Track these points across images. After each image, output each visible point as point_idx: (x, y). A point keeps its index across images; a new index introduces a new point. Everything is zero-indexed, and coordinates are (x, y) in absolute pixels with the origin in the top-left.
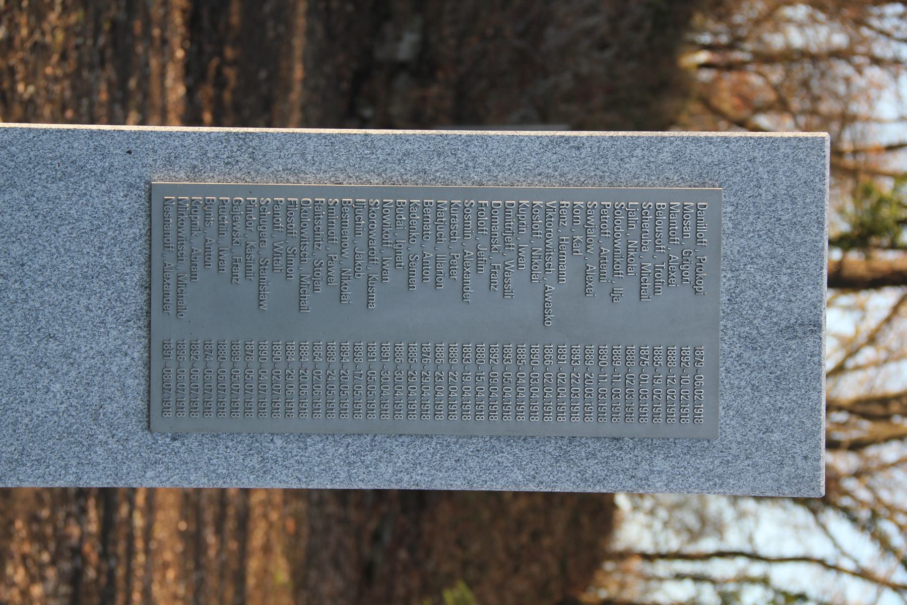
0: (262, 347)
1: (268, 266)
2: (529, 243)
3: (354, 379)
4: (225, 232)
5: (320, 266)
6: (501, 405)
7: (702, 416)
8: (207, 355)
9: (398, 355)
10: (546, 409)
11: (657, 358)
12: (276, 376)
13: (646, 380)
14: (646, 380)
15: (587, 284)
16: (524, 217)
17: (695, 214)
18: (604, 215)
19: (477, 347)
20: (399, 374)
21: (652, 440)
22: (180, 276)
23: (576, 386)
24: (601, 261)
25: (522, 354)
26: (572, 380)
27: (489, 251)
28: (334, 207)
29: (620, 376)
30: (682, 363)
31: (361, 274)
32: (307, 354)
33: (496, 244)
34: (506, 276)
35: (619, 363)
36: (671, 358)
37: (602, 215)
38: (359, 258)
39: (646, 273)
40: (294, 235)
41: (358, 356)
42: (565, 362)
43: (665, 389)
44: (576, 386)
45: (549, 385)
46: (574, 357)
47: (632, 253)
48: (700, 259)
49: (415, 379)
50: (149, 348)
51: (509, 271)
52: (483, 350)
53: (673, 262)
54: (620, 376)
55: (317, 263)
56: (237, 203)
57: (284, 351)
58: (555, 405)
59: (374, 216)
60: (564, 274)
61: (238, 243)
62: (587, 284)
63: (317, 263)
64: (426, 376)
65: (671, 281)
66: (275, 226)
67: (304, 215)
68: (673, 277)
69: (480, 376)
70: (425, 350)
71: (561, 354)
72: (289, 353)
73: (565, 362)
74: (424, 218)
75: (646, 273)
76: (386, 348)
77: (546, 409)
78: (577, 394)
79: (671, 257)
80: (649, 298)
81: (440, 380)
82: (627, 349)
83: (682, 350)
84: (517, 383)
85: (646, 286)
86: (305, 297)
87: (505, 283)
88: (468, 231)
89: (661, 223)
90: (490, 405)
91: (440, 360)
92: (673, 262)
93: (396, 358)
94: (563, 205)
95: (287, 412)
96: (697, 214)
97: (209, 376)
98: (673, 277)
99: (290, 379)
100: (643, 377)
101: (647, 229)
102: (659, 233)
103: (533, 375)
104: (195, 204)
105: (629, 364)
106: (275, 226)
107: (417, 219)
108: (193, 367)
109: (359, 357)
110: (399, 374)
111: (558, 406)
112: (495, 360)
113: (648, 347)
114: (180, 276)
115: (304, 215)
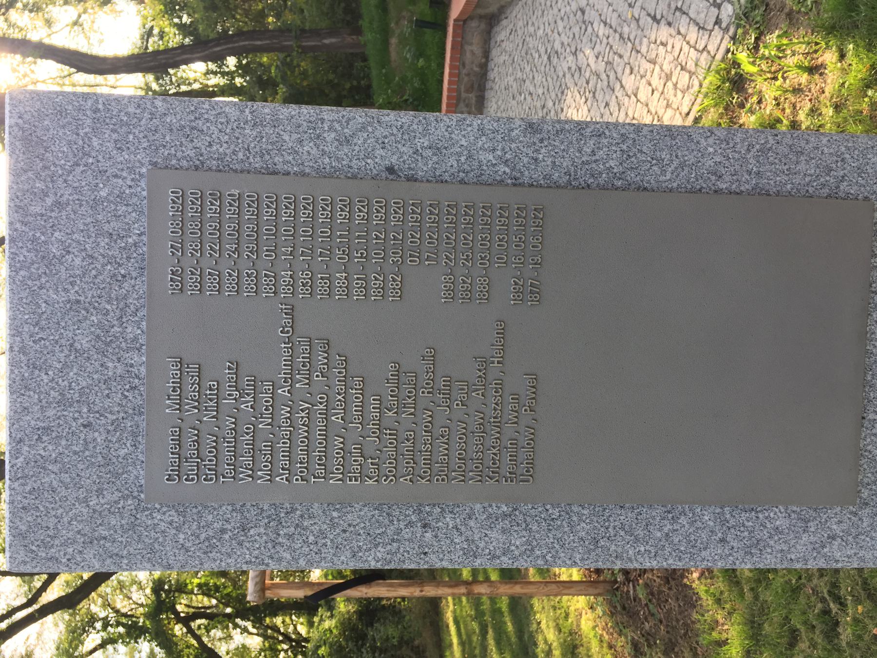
0: (518, 296)
2: (184, 418)
6: (423, 222)
12: (415, 238)
13: (267, 250)
14: (267, 250)
15: (484, 374)
16: (407, 463)
19: (382, 296)
20: (395, 260)
24: (216, 392)
26: (218, 248)
31: (282, 445)
32: (480, 280)
36: (484, 288)
39: (303, 374)
41: (448, 285)
47: (410, 401)
48: (322, 377)
49: (247, 247)
53: (479, 390)
56: (191, 477)
60: (338, 381)
62: (484, 374)
64: (250, 252)
65: (482, 366)
69: (361, 257)
70: (535, 297)
71: (449, 290)
72: (343, 283)
73: (355, 277)
75: (303, 374)
76: (341, 292)
79: (288, 393)
80: (299, 341)
82: (364, 295)
83: (292, 293)
85: (303, 358)
86: (173, 382)
89: (264, 466)
91: (305, 276)
92: (479, 390)
100: (271, 256)
101: (320, 418)
105: (485, 281)
107: (261, 470)
108: (485, 269)
109: (447, 282)
110: (395, 260)
111: (366, 220)
112: (376, 279)
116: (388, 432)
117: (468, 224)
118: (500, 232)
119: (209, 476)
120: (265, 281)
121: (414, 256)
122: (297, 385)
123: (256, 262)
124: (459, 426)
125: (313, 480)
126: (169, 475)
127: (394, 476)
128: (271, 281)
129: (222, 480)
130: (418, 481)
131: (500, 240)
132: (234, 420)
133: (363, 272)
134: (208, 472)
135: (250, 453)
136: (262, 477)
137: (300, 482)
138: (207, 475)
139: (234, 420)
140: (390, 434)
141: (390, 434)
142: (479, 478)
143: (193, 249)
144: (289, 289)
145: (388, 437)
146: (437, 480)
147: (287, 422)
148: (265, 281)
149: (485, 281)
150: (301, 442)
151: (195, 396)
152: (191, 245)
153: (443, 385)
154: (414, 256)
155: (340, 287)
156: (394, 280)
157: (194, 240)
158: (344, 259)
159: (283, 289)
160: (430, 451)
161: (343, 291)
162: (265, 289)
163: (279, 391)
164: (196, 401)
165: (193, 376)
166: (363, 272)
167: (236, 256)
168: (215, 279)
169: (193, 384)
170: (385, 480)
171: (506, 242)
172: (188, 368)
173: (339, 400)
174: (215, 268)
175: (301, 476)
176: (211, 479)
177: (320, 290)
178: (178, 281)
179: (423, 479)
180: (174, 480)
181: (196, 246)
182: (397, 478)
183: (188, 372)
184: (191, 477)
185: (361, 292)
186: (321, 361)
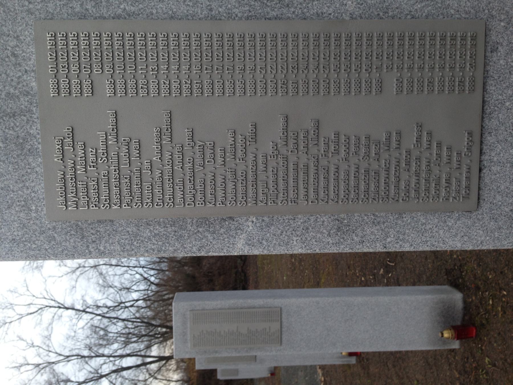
3: (233, 66)
17: (248, 198)
21: (193, 19)
27: (142, 169)
28: (158, 201)
29: (140, 72)
30: (190, 82)
40: (81, 183)
43: (91, 61)
50: (484, 90)
54: (140, 72)
56: (159, 204)
66: (459, 181)
67: (149, 195)
74: (427, 190)
84: (190, 65)
88: (159, 183)
97: (197, 68)
99: (109, 65)
102: (170, 187)
103: (65, 71)
104: (212, 202)
105: (122, 82)
106: (459, 181)
113: (63, 95)
115: (149, 195)
141: (82, 185)
154: (88, 68)
156: (164, 83)
175: (95, 204)
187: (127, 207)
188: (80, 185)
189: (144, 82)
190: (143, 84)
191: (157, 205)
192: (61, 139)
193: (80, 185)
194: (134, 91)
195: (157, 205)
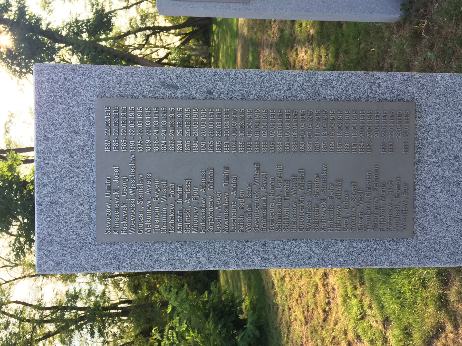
1: (138, 200)
4: (396, 216)
5: (139, 201)
7: (105, 111)
8: (165, 144)
9: (196, 146)
10: (133, 114)
11: (117, 144)
12: (273, 134)
18: (149, 181)
22: (303, 189)
23: (131, 128)
25: (257, 148)
33: (124, 207)
34: (166, 193)
35: (147, 142)
37: (150, 181)
38: (279, 199)
42: (225, 143)
44: (123, 128)
45: (123, 128)
46: (133, 145)
51: (164, 196)
52: (114, 148)
55: (141, 202)
57: (238, 147)
58: (184, 117)
59: (226, 228)
61: (148, 219)
63: (141, 202)
68: (219, 198)
72: (235, 146)
77: (133, 114)
78: (106, 123)
81: (140, 130)
83: (118, 150)
87: (166, 189)
89: (116, 178)
90: (182, 117)
91: (156, 143)
93: (158, 143)
94: (125, 232)
95: (228, 112)
96: (119, 230)
98: (219, 198)
107: (147, 228)
108: (303, 138)
111: (118, 116)
114: (303, 189)
116: (285, 209)
117: (265, 118)
118: (234, 121)
119: (140, 231)
120: (106, 144)
121: (303, 134)
122: (208, 189)
123: (118, 136)
124: (293, 204)
125: (169, 232)
126: (163, 230)
127: (281, 229)
128: (109, 144)
129: (169, 232)
130: (208, 231)
131: (115, 123)
132: (110, 205)
133: (205, 141)
134: (263, 227)
135: (189, 226)
136: (194, 230)
137: (241, 232)
138: (139, 230)
139: (110, 205)
140: (286, 210)
141: (286, 210)
142: (150, 231)
143: (203, 133)
144: (173, 149)
145: (285, 211)
146: (344, 230)
147: (204, 205)
148: (106, 144)
149: (295, 143)
150: (124, 186)
151: (165, 194)
152: (210, 132)
153: (271, 188)
154: (303, 134)
155: (195, 147)
157: (195, 129)
158: (281, 136)
159: (131, 148)
160: (190, 217)
161: (280, 149)
162: (123, 148)
163: (146, 192)
164: (166, 196)
165: (164, 185)
166: (205, 141)
167: (166, 135)
168: (109, 144)
169: (188, 188)
170: (185, 232)
171: (213, 125)
172: (162, 182)
173: (219, 200)
174: (132, 140)
176: (141, 232)
177: (233, 149)
178: (189, 147)
179: (225, 231)
180: (165, 232)
181: (196, 132)
182: (191, 231)
183: (162, 184)
184: (140, 231)
185: (173, 149)
186: (140, 179)
187: (264, 189)
188: (284, 210)
189: (250, 143)
190: (249, 145)
191: (138, 232)
192: (190, 181)
193: (284, 210)
194: (258, 149)
195: (138, 232)
